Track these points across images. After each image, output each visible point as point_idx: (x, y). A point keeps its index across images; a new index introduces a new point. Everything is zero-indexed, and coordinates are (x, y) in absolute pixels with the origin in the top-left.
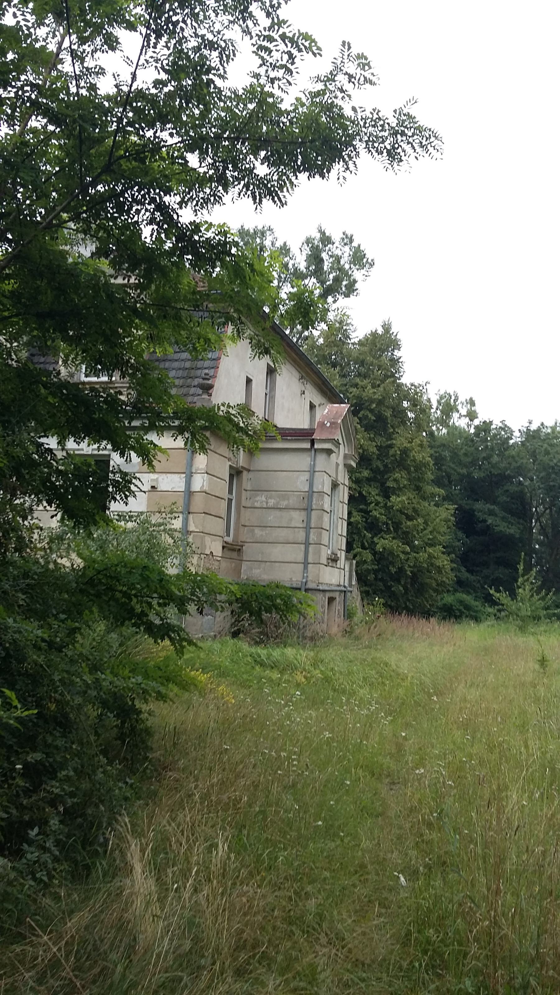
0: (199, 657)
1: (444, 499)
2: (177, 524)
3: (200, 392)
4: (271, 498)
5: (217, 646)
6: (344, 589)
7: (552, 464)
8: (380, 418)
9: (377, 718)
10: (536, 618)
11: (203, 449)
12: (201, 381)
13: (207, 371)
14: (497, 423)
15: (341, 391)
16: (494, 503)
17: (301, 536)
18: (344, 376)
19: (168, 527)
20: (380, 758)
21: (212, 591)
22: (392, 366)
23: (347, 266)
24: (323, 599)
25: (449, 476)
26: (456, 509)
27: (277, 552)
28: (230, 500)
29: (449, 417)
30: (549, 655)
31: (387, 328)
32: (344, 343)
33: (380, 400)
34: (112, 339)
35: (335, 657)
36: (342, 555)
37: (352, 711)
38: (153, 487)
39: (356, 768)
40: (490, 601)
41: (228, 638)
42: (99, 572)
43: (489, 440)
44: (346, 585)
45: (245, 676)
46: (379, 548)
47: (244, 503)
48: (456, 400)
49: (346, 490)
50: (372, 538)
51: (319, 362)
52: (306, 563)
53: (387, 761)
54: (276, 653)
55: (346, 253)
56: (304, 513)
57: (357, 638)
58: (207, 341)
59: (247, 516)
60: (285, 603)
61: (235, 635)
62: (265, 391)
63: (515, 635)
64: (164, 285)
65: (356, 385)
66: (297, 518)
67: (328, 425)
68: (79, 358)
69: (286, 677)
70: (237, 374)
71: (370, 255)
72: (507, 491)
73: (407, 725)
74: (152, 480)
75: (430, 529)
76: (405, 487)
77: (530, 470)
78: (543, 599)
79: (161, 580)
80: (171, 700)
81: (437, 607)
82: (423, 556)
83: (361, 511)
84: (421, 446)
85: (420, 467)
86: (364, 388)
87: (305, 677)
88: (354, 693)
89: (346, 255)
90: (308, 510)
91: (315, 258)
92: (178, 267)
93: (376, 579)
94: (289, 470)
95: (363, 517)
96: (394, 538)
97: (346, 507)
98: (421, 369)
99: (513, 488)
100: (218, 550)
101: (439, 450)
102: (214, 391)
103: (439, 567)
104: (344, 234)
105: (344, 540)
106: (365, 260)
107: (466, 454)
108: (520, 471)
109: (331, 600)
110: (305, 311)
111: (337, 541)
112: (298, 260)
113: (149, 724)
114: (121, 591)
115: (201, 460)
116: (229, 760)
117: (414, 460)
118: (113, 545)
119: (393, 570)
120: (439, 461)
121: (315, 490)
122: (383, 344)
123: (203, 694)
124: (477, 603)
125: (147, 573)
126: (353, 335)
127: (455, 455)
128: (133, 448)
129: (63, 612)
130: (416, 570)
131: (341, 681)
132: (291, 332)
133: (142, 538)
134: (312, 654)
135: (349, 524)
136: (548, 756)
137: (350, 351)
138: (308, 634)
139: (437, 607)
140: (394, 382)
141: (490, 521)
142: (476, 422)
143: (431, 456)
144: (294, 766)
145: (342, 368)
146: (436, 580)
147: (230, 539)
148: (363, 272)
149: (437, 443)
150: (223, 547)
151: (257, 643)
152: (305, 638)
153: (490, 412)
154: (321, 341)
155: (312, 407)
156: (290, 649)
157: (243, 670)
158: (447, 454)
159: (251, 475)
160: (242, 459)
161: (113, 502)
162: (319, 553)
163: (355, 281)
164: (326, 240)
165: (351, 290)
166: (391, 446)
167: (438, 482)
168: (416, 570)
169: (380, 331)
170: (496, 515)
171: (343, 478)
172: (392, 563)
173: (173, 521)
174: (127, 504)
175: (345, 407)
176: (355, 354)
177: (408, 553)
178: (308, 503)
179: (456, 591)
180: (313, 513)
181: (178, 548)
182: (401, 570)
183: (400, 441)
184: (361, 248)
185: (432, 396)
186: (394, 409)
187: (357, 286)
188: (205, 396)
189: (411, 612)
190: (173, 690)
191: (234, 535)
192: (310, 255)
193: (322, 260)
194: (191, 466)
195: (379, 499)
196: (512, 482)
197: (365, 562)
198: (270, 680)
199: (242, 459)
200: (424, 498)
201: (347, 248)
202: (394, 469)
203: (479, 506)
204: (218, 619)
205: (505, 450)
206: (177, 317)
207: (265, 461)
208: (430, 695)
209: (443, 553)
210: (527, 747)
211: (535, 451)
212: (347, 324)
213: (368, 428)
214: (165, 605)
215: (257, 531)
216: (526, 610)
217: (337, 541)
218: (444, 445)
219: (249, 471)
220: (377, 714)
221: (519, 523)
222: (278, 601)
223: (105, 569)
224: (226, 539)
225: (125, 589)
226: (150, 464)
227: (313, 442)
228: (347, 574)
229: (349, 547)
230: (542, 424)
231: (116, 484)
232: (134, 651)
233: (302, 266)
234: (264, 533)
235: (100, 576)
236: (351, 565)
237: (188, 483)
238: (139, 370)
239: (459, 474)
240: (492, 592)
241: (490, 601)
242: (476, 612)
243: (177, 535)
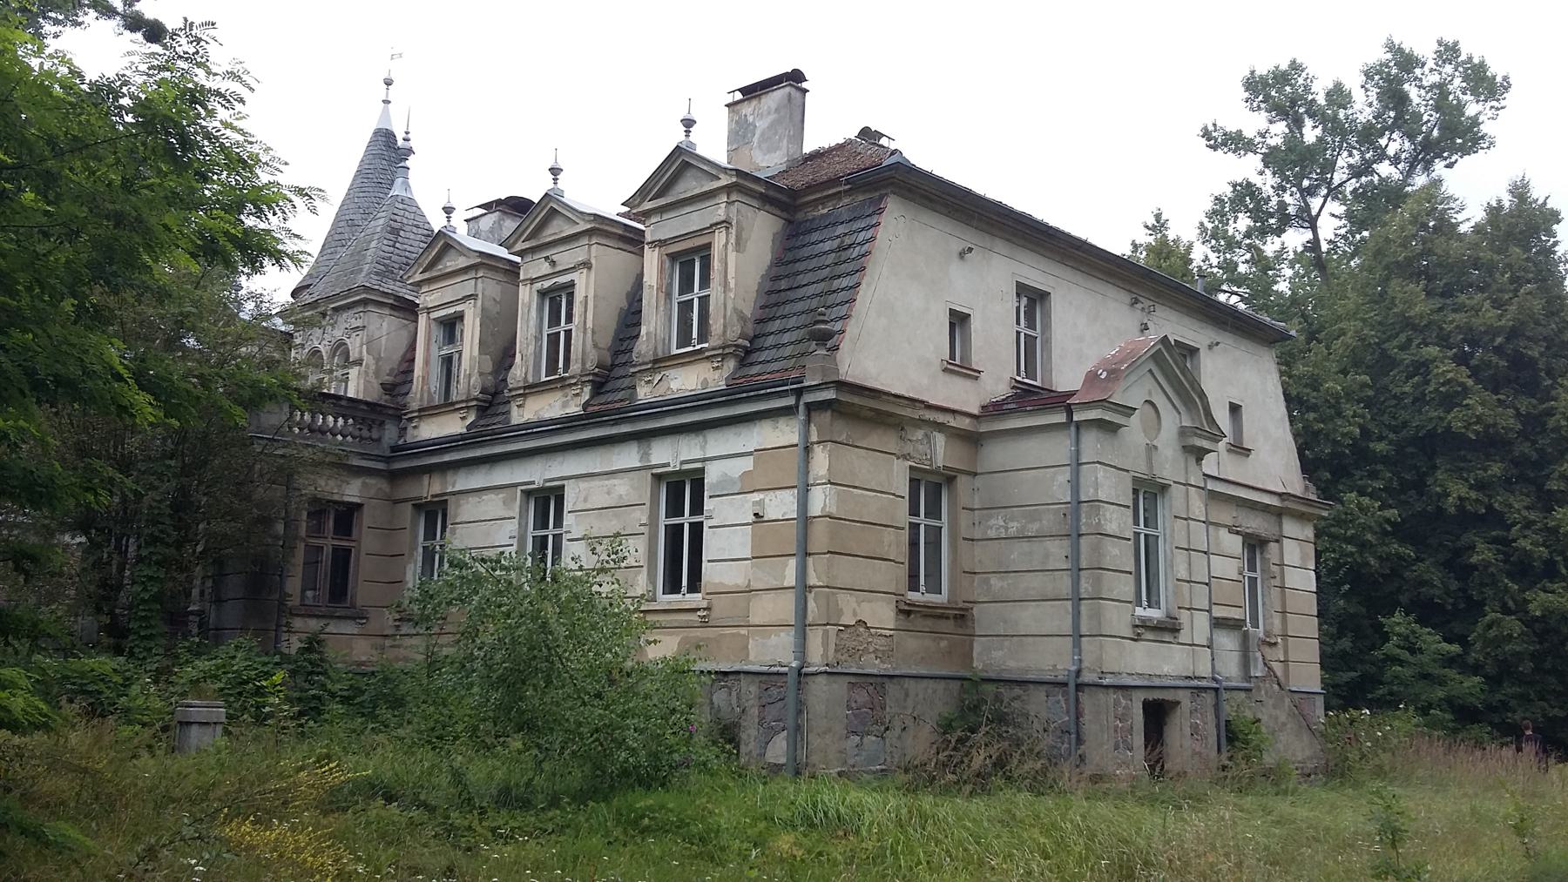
4: (1012, 520)
8: (1519, 362)
17: (1064, 584)
27: (1028, 618)
38: (756, 515)
52: (1077, 636)
56: (1066, 543)
59: (981, 556)
66: (1057, 551)
71: (1496, 69)
74: (755, 503)
83: (1494, 541)
86: (1476, 310)
91: (1393, 96)
100: (882, 615)
121: (1083, 498)
159: (978, 481)
164: (1407, 62)
166: (1550, 413)
180: (1083, 540)
215: (995, 582)
234: (1005, 584)
237: (803, 504)
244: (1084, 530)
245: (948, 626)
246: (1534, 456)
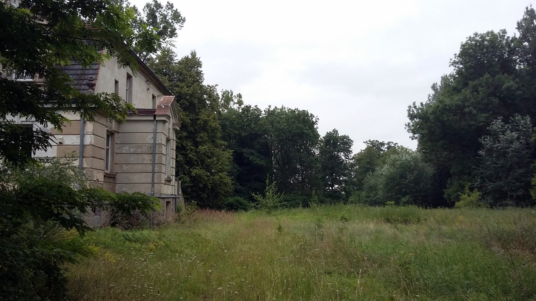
0: (92, 239)
1: (227, 147)
2: (76, 163)
3: (88, 88)
4: (132, 148)
5: (102, 232)
6: (174, 196)
7: (281, 128)
8: (192, 104)
9: (195, 264)
10: (276, 207)
11: (91, 119)
12: (88, 81)
13: (91, 76)
14: (253, 106)
15: (169, 89)
16: (253, 148)
17: (150, 168)
18: (171, 81)
19: (71, 165)
20: (198, 284)
21: (100, 199)
22: (197, 76)
23: (170, 21)
24: (163, 203)
25: (229, 135)
26: (234, 152)
27: (136, 178)
28: (108, 150)
29: (228, 104)
30: (283, 226)
31: (194, 54)
32: (170, 63)
33: (191, 94)
34: (33, 55)
35: (171, 234)
36: (173, 178)
37: (182, 261)
39: (185, 291)
40: (253, 200)
41: (109, 227)
42: (30, 191)
43: (249, 115)
44: (176, 194)
45: (120, 248)
46: (193, 174)
47: (116, 151)
48: (232, 95)
49: (175, 142)
50: (189, 169)
51: (156, 73)
52: (153, 183)
53: (202, 286)
54: (138, 234)
55: (169, 14)
56: (151, 156)
57: (183, 223)
58: (92, 57)
59: (117, 158)
60: (144, 204)
61: (113, 225)
62: (126, 88)
63: (265, 216)
64: (65, 25)
65: (178, 86)
67: (163, 107)
68: (13, 65)
69: (144, 246)
70: (109, 77)
71: (183, 15)
72: (259, 142)
73: (212, 266)
75: (220, 163)
76: (206, 141)
77: (270, 131)
78: (278, 197)
79: (70, 193)
80: (78, 262)
81: (225, 205)
82: (217, 177)
83: (183, 154)
84: (214, 119)
85: (214, 130)
86: (182, 87)
87: (155, 246)
88: (183, 252)
89: (170, 14)
90: (153, 154)
91: (152, 15)
92: (73, 14)
93: (192, 191)
94: (142, 132)
95: (184, 158)
96: (201, 169)
97: (175, 152)
98: (215, 76)
99: (262, 141)
101: (224, 121)
102: (96, 88)
103: (225, 183)
104: (168, 3)
105: (174, 170)
106: (180, 18)
107: (237, 123)
108: (266, 132)
109: (168, 203)
110: (149, 43)
111: (170, 171)
112: (142, 16)
113: (65, 275)
114: (44, 201)
115: (90, 126)
116: (113, 292)
117: (211, 127)
118: (36, 176)
119: (201, 186)
120: (223, 126)
121: (157, 143)
122: (192, 64)
123: (96, 258)
124: (245, 201)
125: (61, 189)
126: (175, 58)
127: (232, 123)
128: (48, 119)
129: (10, 214)
130: (213, 185)
131: (175, 246)
132: (140, 56)
133: (55, 172)
134: (158, 233)
135: (177, 161)
136: (285, 275)
137: (173, 68)
138: (156, 222)
139: (225, 205)
140: (199, 84)
141: (251, 158)
142: (243, 106)
143: (220, 124)
144: (151, 292)
145: (170, 77)
146: (224, 190)
147: (108, 172)
148: (179, 24)
149: (222, 118)
150: (105, 176)
151: (126, 229)
152: (153, 224)
153: (248, 101)
154: (157, 61)
155: (154, 97)
156: (145, 231)
157: (119, 244)
158: (227, 123)
159: (120, 135)
160: (114, 126)
161: (37, 150)
162: (160, 177)
163: (175, 29)
164: (158, 6)
165: (173, 34)
166: (198, 119)
167: (223, 138)
168: (213, 185)
169: (190, 57)
170: (254, 155)
171: (173, 136)
172: (201, 182)
173: (74, 162)
174: (46, 151)
175: (172, 98)
176: (177, 69)
177: (209, 176)
178: (153, 150)
179: (234, 195)
181: (77, 177)
182: (205, 186)
183: (203, 116)
184: (178, 11)
185: (219, 92)
186: (199, 99)
187: (176, 31)
188: (91, 90)
189: (211, 208)
190: (79, 257)
191: (111, 169)
192: (149, 14)
193: (156, 17)
194: (84, 130)
195: (193, 148)
196: (262, 138)
197: (186, 182)
198: (135, 249)
199: (114, 126)
200: (217, 147)
201: (170, 11)
202: (200, 132)
203: (245, 150)
204: (102, 217)
205: (258, 121)
206: (74, 43)
207: (127, 127)
208: (223, 250)
209: (227, 176)
210: (274, 271)
211: (272, 122)
212: (172, 52)
213: (185, 109)
214: (72, 208)
215: (124, 166)
216: (270, 203)
217: (170, 171)
218: (226, 118)
219: (118, 133)
220: (196, 262)
221: (266, 159)
222: (140, 202)
223: (35, 189)
224: (106, 171)
225: (47, 200)
226: (59, 128)
227: (155, 117)
228: (176, 188)
229: (177, 175)
230: (276, 107)
231: (39, 139)
232: (53, 237)
233: (145, 19)
235: (31, 193)
236: (178, 183)
237: (82, 140)
238: (50, 73)
239: (234, 133)
240: (253, 195)
241: (253, 200)
242: (245, 206)
243: (76, 170)
244: (157, 152)
245: (111, 180)
246: (194, 131)
